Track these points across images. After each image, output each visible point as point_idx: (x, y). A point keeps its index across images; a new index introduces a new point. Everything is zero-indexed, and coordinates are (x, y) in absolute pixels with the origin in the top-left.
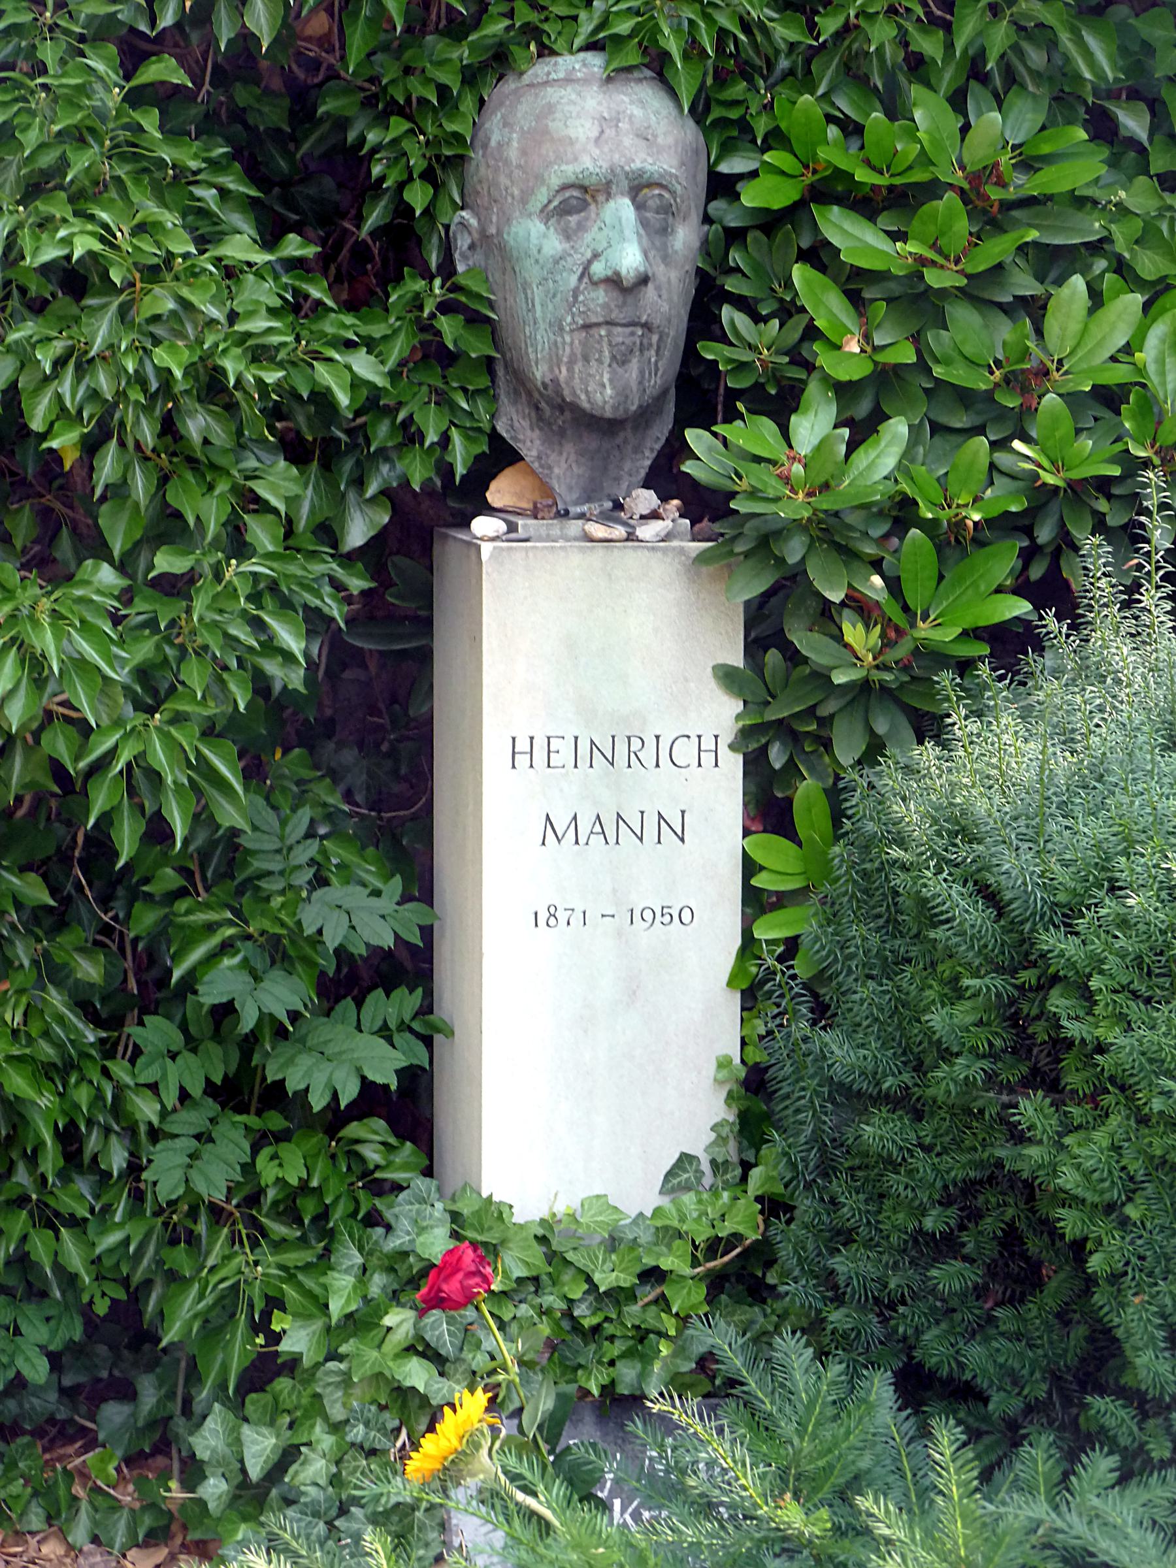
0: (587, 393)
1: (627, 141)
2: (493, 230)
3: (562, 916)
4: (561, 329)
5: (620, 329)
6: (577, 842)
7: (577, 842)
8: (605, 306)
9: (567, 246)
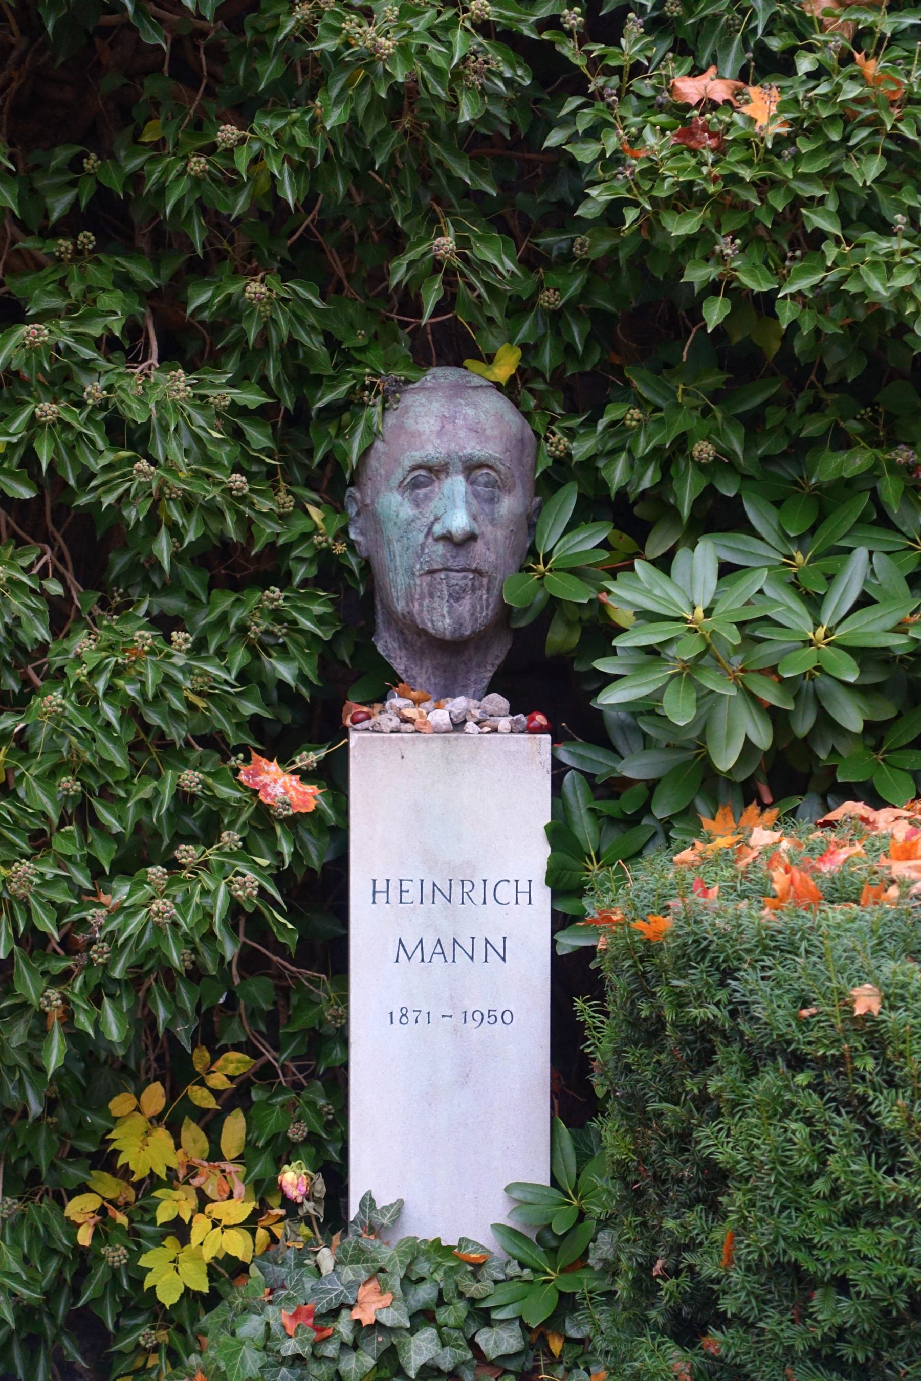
0: (432, 622)
1: (462, 434)
2: (368, 501)
3: (412, 1016)
4: (413, 574)
5: (455, 574)
6: (423, 960)
7: (423, 960)
8: (444, 556)
9: (416, 511)
